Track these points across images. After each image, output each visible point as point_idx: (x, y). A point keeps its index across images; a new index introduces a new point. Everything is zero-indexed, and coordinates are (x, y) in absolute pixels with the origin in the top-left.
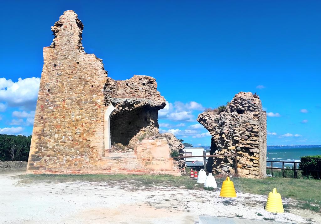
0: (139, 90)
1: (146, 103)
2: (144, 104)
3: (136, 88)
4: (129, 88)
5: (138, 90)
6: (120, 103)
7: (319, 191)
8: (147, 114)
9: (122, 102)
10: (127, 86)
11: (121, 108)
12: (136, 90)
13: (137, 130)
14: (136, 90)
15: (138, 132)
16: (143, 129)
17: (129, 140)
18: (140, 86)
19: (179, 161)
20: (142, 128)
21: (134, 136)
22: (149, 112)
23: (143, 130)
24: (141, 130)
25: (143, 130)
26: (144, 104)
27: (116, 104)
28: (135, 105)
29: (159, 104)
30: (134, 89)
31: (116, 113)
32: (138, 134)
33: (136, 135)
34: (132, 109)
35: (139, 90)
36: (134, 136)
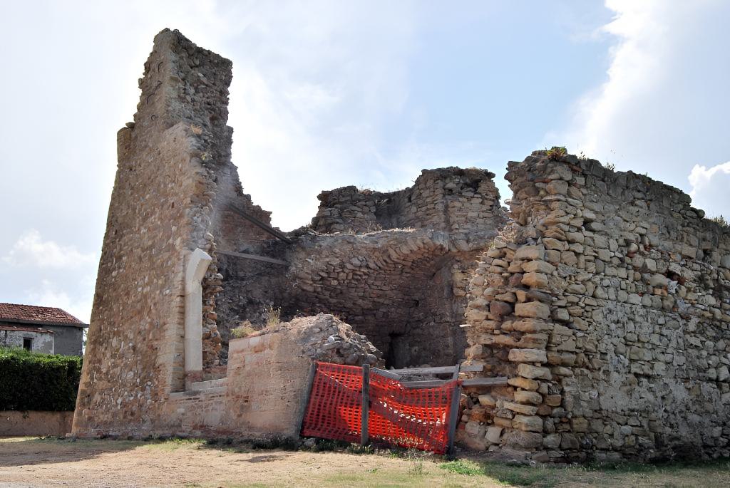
0: (434, 208)
3: (428, 207)
10: (409, 204)
14: (428, 212)
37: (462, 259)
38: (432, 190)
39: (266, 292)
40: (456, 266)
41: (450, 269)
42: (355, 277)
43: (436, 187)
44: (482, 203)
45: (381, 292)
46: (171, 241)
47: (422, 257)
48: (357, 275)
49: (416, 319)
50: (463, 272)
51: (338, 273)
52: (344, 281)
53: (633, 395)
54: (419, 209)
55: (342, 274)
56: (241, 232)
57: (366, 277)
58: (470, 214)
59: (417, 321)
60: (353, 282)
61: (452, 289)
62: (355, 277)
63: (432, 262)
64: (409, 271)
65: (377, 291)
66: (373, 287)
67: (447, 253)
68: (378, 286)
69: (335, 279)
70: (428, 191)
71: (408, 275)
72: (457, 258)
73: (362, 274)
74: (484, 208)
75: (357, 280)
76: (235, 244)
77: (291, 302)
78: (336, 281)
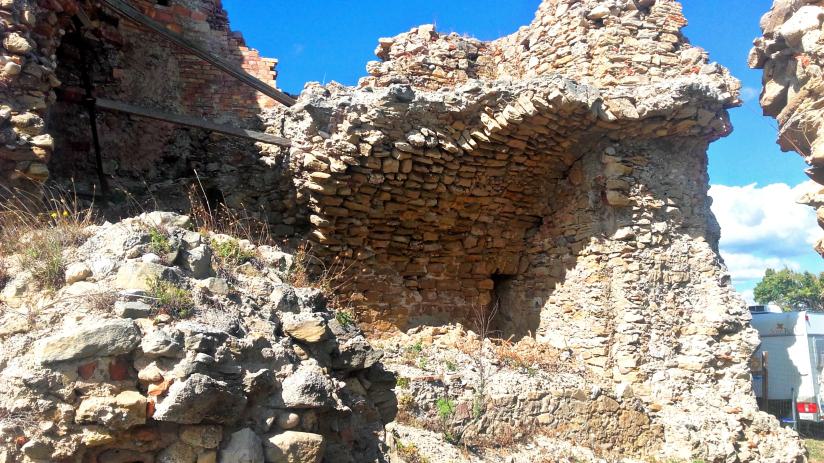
0: (569, 53)
1: (551, 97)
2: (535, 103)
3: (559, 52)
4: (534, 61)
5: (567, 58)
6: (364, 109)
7: (249, 102)
8: (604, 165)
9: (375, 102)
10: (527, 53)
11: (374, 137)
12: (559, 61)
13: (567, 256)
14: (559, 61)
15: (572, 265)
16: (593, 246)
17: (539, 306)
18: (572, 35)
19: (326, 311)
20: (586, 242)
21: (558, 286)
22: (619, 153)
23: (591, 253)
24: (584, 252)
25: (591, 253)
26: (535, 103)
27: (340, 118)
28: (484, 118)
29: (659, 97)
30: (553, 56)
31: (345, 163)
32: (571, 274)
33: (562, 279)
34: (473, 142)
35: (569, 53)
36: (558, 286)
37: (622, 137)
38: (565, 21)
39: (256, 198)
40: (610, 150)
41: (599, 157)
42: (417, 169)
43: (572, 15)
44: (657, 39)
45: (471, 200)
46: (318, 209)
47: (546, 132)
48: (420, 164)
49: (539, 249)
50: (623, 161)
51: (383, 159)
52: (396, 175)
53: (62, 312)
54: (542, 60)
55: (387, 163)
56: (216, 92)
57: (441, 170)
58: (637, 57)
59: (540, 253)
60: (414, 177)
61: (604, 194)
62: (417, 169)
63: (565, 145)
64: (522, 160)
65: (465, 199)
66: (454, 189)
67: (593, 124)
68: (464, 188)
69: (375, 172)
70: (558, 25)
71: (522, 168)
72: (613, 136)
73: (430, 162)
74: (662, 46)
75: (423, 175)
76: (205, 114)
77: (298, 216)
78: (378, 176)
